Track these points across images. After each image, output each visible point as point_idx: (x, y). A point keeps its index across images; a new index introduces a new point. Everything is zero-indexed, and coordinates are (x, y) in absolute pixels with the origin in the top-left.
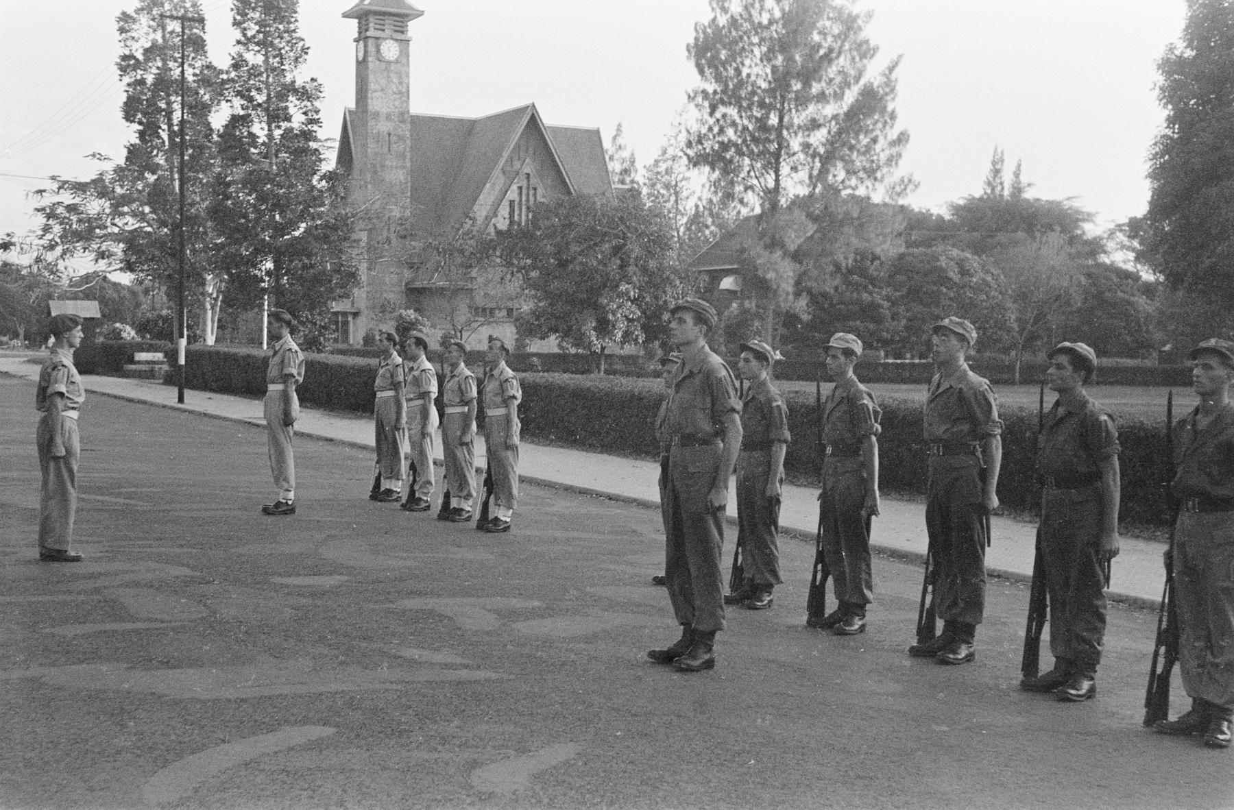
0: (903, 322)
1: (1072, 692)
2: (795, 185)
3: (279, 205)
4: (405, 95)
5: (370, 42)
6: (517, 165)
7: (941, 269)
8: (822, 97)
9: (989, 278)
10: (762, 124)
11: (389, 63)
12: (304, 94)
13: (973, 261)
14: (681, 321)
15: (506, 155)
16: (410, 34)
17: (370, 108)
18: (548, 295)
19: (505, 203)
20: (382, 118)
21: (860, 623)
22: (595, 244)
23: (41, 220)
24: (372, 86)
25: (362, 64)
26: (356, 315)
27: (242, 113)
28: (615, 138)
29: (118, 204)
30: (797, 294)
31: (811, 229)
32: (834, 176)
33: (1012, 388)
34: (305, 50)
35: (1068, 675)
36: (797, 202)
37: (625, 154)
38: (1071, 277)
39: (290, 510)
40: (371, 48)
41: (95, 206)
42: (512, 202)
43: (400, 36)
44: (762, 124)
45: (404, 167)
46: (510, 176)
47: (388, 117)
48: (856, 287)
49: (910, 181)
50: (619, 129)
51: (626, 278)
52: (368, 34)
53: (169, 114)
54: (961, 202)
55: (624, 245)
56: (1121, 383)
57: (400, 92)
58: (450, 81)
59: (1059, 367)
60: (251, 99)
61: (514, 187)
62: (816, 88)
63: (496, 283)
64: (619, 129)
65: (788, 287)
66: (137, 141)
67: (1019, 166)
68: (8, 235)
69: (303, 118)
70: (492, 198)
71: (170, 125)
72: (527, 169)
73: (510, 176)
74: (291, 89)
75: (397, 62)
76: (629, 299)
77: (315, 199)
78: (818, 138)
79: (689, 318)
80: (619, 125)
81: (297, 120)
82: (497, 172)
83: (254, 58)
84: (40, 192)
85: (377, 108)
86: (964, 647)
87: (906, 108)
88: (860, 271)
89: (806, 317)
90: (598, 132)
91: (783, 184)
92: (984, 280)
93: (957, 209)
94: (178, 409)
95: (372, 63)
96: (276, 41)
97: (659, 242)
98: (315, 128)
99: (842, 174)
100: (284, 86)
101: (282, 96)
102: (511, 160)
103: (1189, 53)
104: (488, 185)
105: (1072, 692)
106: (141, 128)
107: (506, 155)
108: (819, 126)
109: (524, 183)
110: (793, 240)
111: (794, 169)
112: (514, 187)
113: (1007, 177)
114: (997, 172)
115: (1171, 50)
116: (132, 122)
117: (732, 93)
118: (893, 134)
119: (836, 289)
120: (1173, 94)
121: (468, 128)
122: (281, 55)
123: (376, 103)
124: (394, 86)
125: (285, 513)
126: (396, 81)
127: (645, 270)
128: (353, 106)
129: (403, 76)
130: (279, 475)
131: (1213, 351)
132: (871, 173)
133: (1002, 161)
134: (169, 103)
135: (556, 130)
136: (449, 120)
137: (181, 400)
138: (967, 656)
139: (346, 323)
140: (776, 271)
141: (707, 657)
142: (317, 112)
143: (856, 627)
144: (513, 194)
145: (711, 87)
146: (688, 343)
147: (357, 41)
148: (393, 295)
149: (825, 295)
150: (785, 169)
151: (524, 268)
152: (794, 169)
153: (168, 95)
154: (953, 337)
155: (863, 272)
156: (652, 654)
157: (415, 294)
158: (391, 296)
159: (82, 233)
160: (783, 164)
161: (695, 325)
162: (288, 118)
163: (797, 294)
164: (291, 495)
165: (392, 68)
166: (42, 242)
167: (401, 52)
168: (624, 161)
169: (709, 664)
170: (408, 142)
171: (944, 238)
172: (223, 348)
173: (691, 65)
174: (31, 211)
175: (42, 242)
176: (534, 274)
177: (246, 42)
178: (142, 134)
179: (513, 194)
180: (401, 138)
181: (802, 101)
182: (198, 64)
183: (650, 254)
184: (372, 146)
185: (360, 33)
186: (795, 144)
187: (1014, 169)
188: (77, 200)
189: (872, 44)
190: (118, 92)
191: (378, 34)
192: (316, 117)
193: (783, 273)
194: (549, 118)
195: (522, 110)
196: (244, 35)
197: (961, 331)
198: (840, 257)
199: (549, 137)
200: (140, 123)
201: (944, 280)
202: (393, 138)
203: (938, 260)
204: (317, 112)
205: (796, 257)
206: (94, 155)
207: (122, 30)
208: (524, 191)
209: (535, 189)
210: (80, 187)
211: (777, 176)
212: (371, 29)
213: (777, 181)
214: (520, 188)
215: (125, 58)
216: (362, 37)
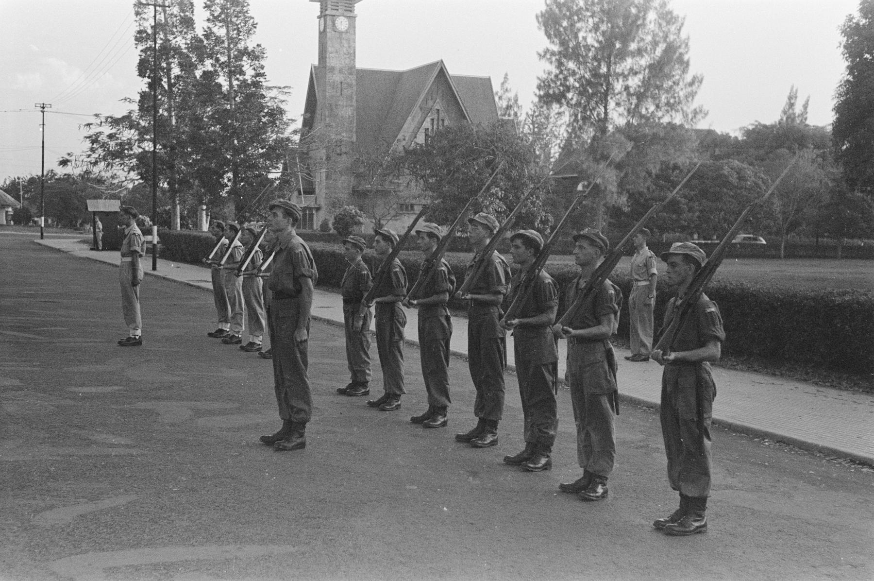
0: (697, 214)
1: (532, 466)
2: (618, 117)
3: (236, 133)
4: (352, 55)
5: (328, 18)
6: (430, 103)
7: (726, 177)
8: (640, 52)
9: (760, 182)
10: (596, 74)
11: (341, 33)
12: (254, 56)
13: (749, 172)
14: (275, 215)
15: (422, 97)
16: (356, 12)
17: (328, 64)
18: (442, 195)
19: (422, 130)
20: (336, 72)
21: (442, 420)
22: (474, 159)
23: (88, 144)
24: (330, 49)
25: (322, 34)
26: (318, 209)
27: (212, 69)
28: (503, 84)
29: (143, 132)
30: (620, 193)
31: (629, 146)
32: (647, 109)
33: (780, 261)
34: (254, 25)
35: (533, 453)
36: (618, 129)
37: (511, 95)
38: (821, 182)
39: (137, 343)
40: (329, 22)
41: (128, 134)
42: (427, 130)
43: (349, 14)
44: (596, 74)
45: (351, 106)
46: (426, 112)
47: (341, 71)
48: (662, 188)
49: (701, 111)
50: (506, 77)
51: (495, 183)
52: (327, 13)
53: (169, 70)
54: (751, 128)
55: (494, 159)
56: (861, 258)
57: (349, 53)
58: (385, 44)
59: (517, 247)
60: (217, 60)
61: (428, 119)
62: (633, 46)
63: (409, 187)
64: (506, 77)
65: (613, 188)
66: (147, 90)
67: (808, 101)
68: (69, 154)
69: (253, 73)
70: (413, 126)
71: (169, 79)
72: (437, 107)
73: (426, 112)
74: (245, 52)
75: (347, 32)
76: (498, 198)
77: (260, 128)
78: (634, 82)
79: (280, 213)
80: (506, 75)
81: (249, 74)
82: (416, 108)
83: (220, 31)
84: (89, 125)
85: (332, 65)
86: (489, 436)
87: (698, 59)
88: (666, 176)
89: (626, 209)
90: (489, 80)
91: (610, 116)
92: (756, 184)
93: (748, 133)
94: (153, 275)
95: (330, 33)
96: (234, 19)
97: (519, 156)
98: (262, 79)
99: (652, 108)
100: (239, 51)
101: (239, 57)
102: (426, 100)
103: (863, 21)
104: (410, 118)
105: (532, 466)
106: (150, 80)
107: (422, 97)
108: (636, 73)
109: (436, 116)
110: (617, 155)
111: (618, 104)
112: (428, 119)
113: (798, 109)
114: (791, 105)
115: (851, 20)
116: (144, 76)
117: (569, 51)
118: (688, 78)
119: (648, 188)
120: (853, 51)
121: (397, 77)
122: (238, 29)
123: (333, 61)
124: (345, 49)
125: (134, 345)
126: (346, 45)
127: (509, 178)
128: (316, 63)
129: (351, 43)
130: (130, 318)
131: (585, 237)
132: (671, 106)
133: (796, 97)
134: (169, 64)
135: (459, 79)
136: (385, 72)
137: (154, 268)
138: (492, 441)
139: (311, 215)
140: (603, 178)
141: (299, 441)
142: (262, 67)
143: (439, 423)
144: (427, 124)
145: (556, 48)
146: (281, 230)
147: (319, 17)
148: (344, 196)
149: (641, 194)
150: (612, 104)
151: (424, 176)
152: (618, 104)
153: (168, 58)
154: (480, 227)
155: (667, 179)
156: (263, 439)
157: (359, 195)
158: (342, 195)
159: (119, 154)
160: (610, 101)
161: (284, 217)
162: (242, 73)
163: (620, 193)
164: (139, 332)
165: (344, 36)
166: (89, 159)
167: (350, 24)
168: (509, 100)
169: (302, 445)
170: (355, 88)
171: (739, 153)
172: (185, 232)
173: (542, 33)
174: (82, 138)
175: (89, 159)
176: (432, 180)
177: (214, 19)
178: (151, 86)
179: (427, 124)
180: (350, 85)
181: (622, 55)
182: (189, 36)
183: (512, 166)
184: (329, 92)
185: (321, 12)
186: (618, 86)
187: (803, 103)
188: (114, 131)
189: (675, 13)
190: (134, 55)
191: (334, 12)
192: (262, 71)
193: (608, 178)
194: (453, 70)
195: (430, 67)
196: (213, 15)
197: (486, 222)
198: (650, 166)
199: (453, 84)
200: (149, 77)
201: (726, 183)
202: (344, 86)
203: (722, 169)
204: (262, 67)
205: (619, 166)
206: (126, 99)
207: (137, 14)
208: (435, 122)
209: (443, 120)
210: (115, 122)
211: (606, 109)
212: (329, 9)
213: (606, 113)
214: (433, 120)
215: (140, 32)
216: (323, 16)
